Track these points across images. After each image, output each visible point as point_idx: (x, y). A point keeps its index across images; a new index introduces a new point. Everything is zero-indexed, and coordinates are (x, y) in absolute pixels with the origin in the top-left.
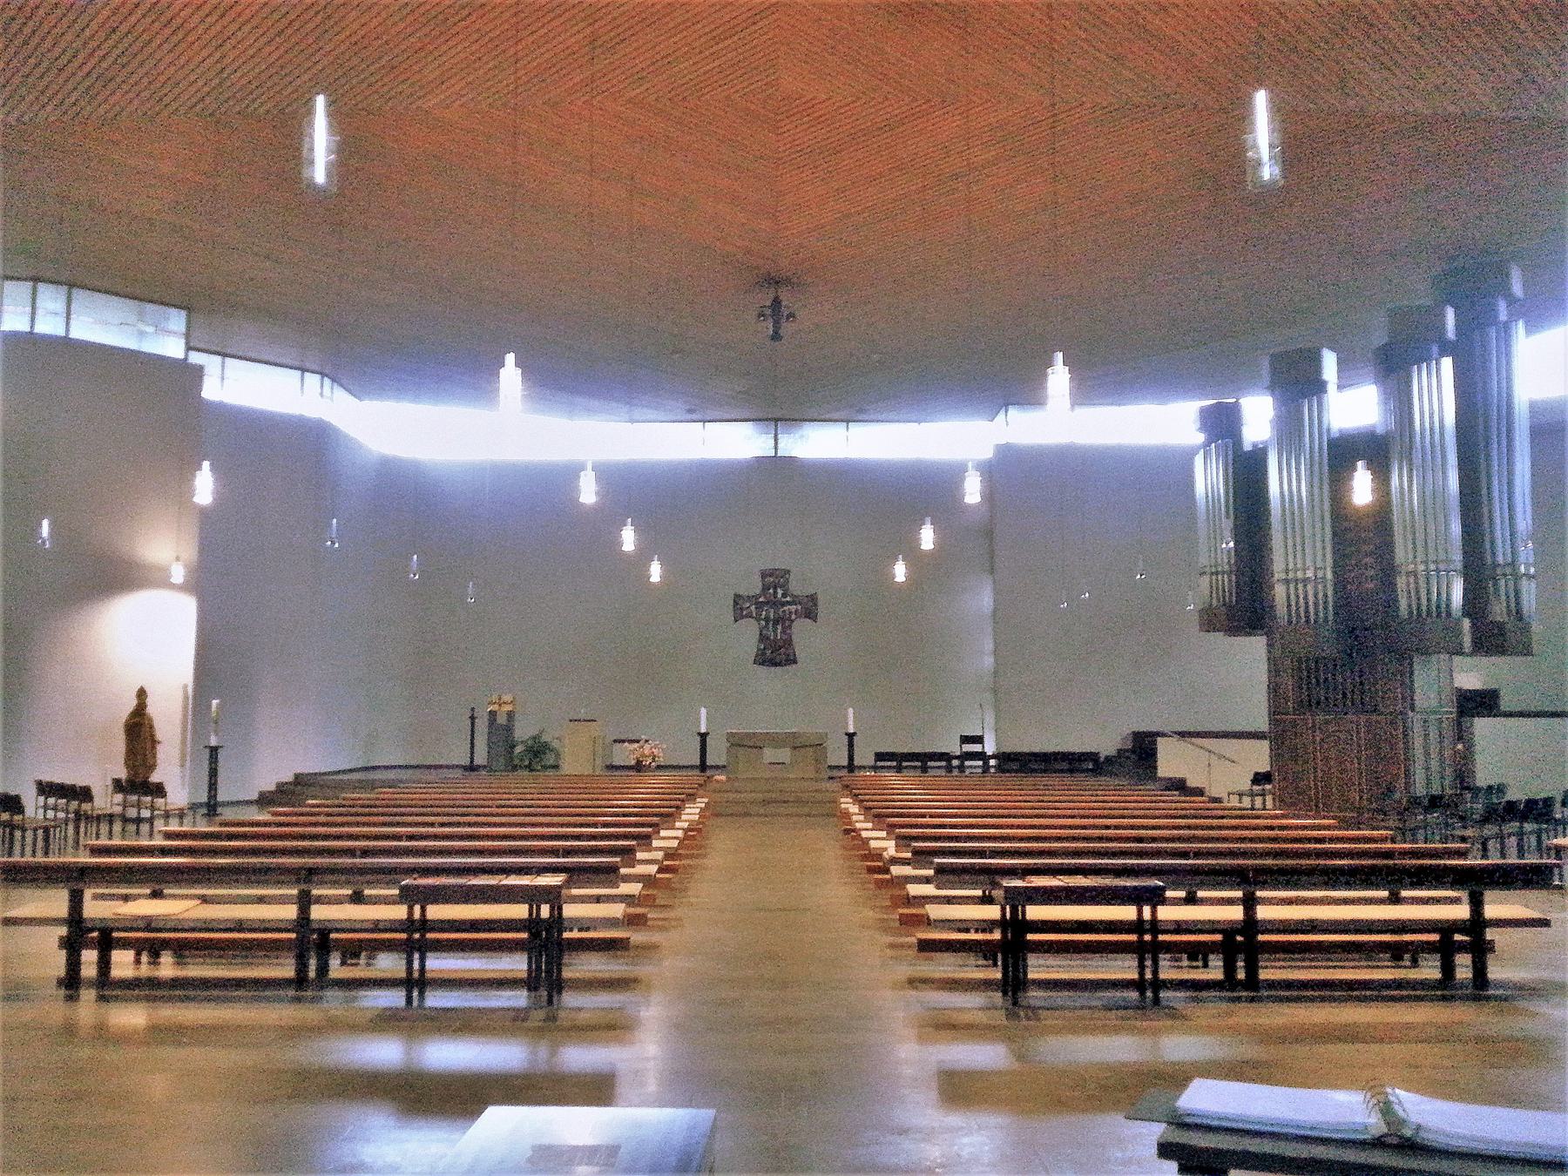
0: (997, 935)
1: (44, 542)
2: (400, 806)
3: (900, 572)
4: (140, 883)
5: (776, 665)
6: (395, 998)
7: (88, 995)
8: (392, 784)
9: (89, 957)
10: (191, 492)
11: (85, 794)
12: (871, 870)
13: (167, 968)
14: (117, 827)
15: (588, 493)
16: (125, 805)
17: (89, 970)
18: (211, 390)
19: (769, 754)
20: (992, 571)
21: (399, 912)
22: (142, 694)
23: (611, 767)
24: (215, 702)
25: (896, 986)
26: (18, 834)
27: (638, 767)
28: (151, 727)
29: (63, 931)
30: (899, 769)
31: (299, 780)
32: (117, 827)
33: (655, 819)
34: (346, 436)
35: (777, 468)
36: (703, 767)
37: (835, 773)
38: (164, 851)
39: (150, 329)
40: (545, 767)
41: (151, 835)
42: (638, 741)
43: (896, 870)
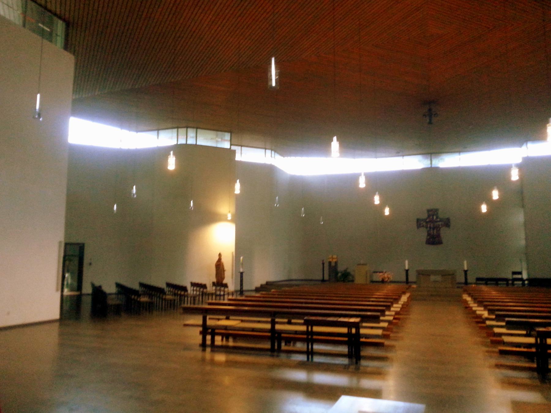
0: (534, 350)
1: (191, 208)
2: (494, 302)
3: (484, 208)
4: (223, 314)
6: (303, 358)
7: (208, 350)
8: (297, 285)
9: (209, 337)
10: (233, 190)
11: (204, 286)
12: (478, 322)
13: (231, 343)
14: (214, 297)
15: (362, 184)
16: (216, 290)
17: (208, 342)
18: (238, 158)
19: (433, 278)
20: (523, 206)
21: (303, 328)
22: (220, 255)
23: (373, 282)
24: (241, 258)
25: (490, 367)
26: (186, 298)
27: (383, 281)
28: (223, 266)
29: (201, 329)
30: (486, 284)
31: (268, 283)
32: (214, 297)
33: (392, 300)
34: (280, 170)
35: (432, 171)
36: (407, 282)
37: (460, 285)
38: (229, 305)
39: (220, 140)
40: (349, 281)
41: (224, 300)
42: (382, 272)
43: (488, 323)
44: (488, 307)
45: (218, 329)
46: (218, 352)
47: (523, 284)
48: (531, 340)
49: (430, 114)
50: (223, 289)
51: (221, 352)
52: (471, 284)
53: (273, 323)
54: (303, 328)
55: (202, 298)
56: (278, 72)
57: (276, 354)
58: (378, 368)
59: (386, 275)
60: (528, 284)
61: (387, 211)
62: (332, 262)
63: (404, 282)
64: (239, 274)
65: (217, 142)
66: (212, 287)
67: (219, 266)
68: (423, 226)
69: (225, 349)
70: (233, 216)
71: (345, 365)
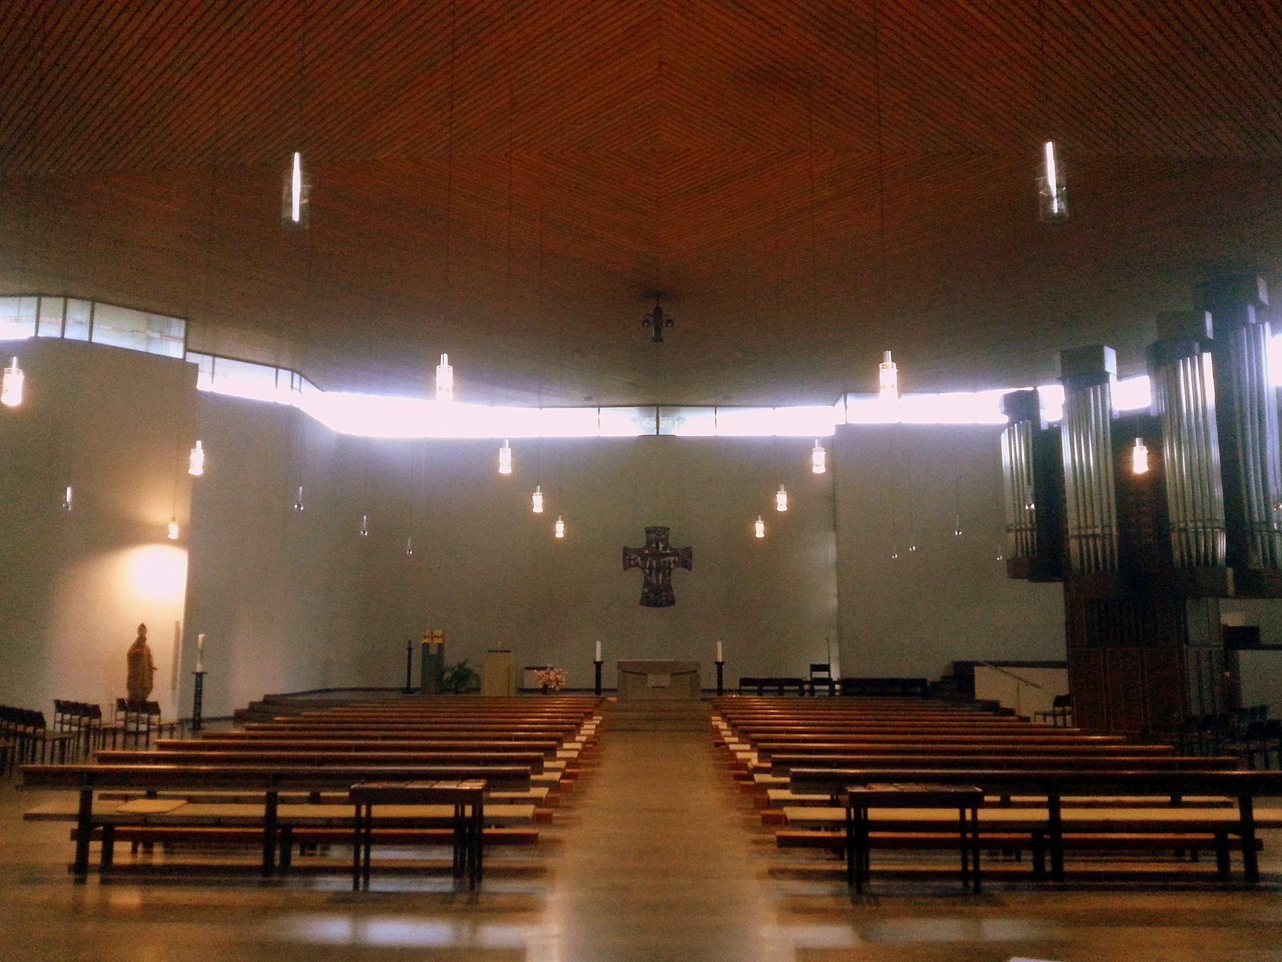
0: (843, 834)
1: (68, 507)
3: (760, 529)
4: (139, 786)
5: (661, 605)
6: (343, 884)
7: (94, 879)
9: (96, 846)
11: (94, 711)
12: (738, 777)
14: (120, 738)
15: (505, 467)
16: (126, 720)
17: (95, 859)
20: (835, 530)
21: (349, 811)
22: (142, 629)
24: (201, 636)
25: (760, 876)
26: (39, 744)
27: (545, 690)
29: (75, 825)
30: (760, 693)
31: (268, 700)
32: (120, 738)
34: (311, 420)
35: (659, 443)
36: (598, 690)
38: (157, 759)
39: (157, 335)
42: (544, 669)
43: (759, 778)
44: (760, 744)
45: (298, 826)
46: (122, 883)
47: (832, 691)
48: (839, 813)
49: (658, 319)
50: (145, 716)
51: (133, 882)
52: (730, 691)
53: (1054, 807)
54: (349, 811)
55: (87, 742)
56: (309, 189)
57: (276, 878)
58: (520, 895)
59: (552, 676)
60: (840, 691)
61: (560, 530)
62: (431, 646)
63: (592, 690)
64: (193, 679)
65: (149, 339)
66: (117, 711)
67: (139, 658)
68: (637, 565)
69: (140, 874)
70: (183, 529)
71: (445, 894)
